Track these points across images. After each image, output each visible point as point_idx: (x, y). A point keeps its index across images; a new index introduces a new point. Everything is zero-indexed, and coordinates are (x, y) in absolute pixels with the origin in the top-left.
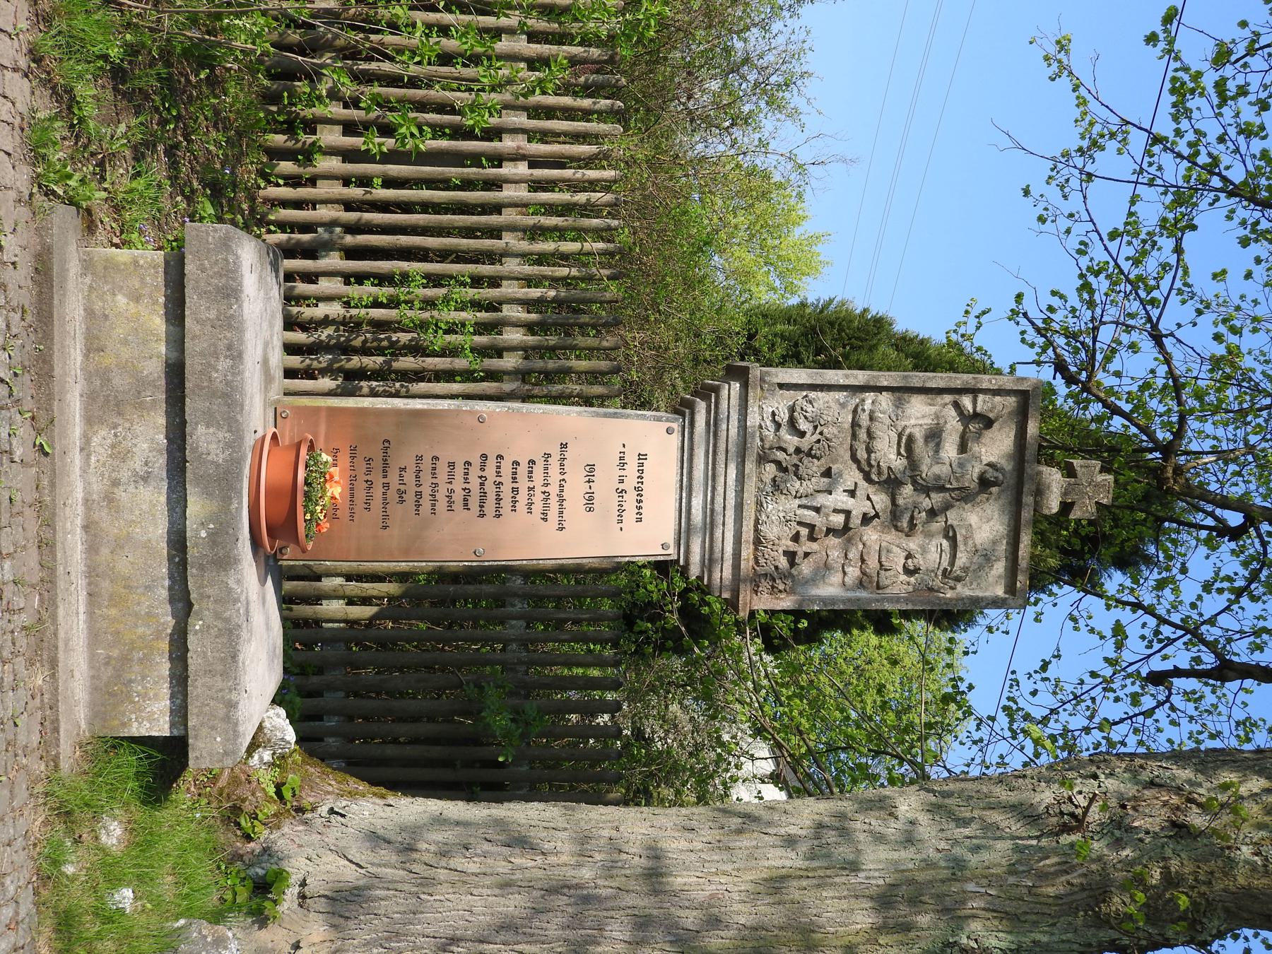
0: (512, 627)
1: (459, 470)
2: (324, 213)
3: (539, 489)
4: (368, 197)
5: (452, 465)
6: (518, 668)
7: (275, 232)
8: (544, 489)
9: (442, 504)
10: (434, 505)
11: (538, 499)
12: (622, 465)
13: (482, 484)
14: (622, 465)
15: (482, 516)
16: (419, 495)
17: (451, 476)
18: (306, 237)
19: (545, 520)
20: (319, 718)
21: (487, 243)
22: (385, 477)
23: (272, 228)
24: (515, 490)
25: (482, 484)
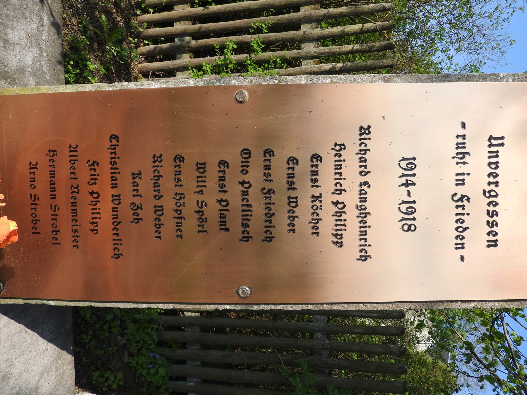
0: (317, 320)
1: (213, 172)
2: (178, 27)
3: (328, 199)
4: (206, 11)
5: (201, 167)
6: (322, 352)
7: (148, 45)
8: (336, 198)
9: (191, 224)
10: (179, 224)
11: (328, 212)
12: (462, 154)
13: (245, 193)
14: (462, 154)
15: (247, 239)
16: (159, 210)
17: (201, 179)
18: (165, 46)
19: (339, 244)
20: (184, 379)
21: (289, 34)
22: (114, 186)
23: (146, 42)
24: (293, 201)
25: (245, 193)
